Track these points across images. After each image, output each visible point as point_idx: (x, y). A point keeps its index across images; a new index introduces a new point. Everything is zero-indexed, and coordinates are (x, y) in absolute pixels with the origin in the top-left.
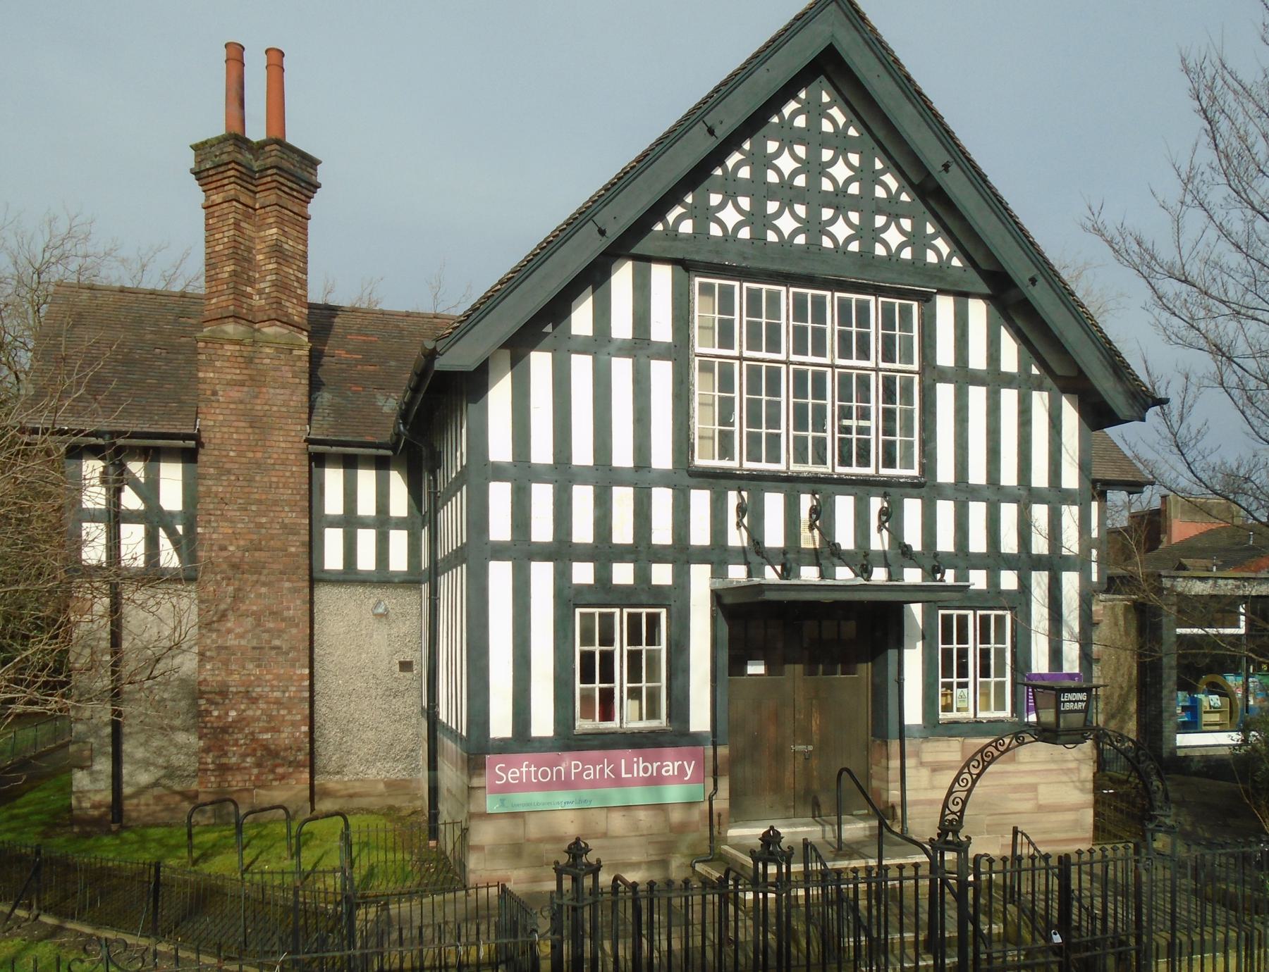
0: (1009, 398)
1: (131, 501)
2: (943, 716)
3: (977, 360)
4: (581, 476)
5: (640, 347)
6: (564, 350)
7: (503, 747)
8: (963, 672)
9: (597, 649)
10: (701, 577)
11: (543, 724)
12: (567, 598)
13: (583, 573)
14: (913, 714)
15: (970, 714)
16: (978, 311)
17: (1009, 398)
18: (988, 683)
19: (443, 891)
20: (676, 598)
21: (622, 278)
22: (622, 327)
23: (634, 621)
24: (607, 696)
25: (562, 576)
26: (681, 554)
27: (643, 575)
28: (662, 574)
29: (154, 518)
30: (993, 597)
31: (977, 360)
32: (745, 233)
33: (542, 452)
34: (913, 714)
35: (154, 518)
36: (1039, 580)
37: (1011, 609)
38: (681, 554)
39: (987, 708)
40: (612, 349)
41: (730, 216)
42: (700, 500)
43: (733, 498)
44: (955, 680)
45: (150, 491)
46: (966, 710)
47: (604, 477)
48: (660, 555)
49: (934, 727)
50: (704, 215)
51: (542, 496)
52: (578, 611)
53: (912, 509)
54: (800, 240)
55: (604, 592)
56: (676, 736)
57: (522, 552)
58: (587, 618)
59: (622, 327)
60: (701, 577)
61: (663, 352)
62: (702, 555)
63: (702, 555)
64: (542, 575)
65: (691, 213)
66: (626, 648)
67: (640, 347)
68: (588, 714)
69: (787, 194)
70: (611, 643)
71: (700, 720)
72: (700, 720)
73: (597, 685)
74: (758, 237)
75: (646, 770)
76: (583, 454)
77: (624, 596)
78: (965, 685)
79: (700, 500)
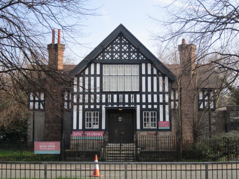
0: (155, 78)
1: (37, 99)
2: (144, 128)
3: (149, 72)
4: (149, 93)
5: (95, 75)
6: (84, 76)
7: (75, 130)
8: (148, 121)
9: (89, 117)
10: (104, 106)
11: (80, 127)
12: (84, 110)
13: (86, 107)
14: (138, 127)
15: (149, 128)
16: (149, 65)
17: (155, 78)
18: (153, 123)
19: (164, 152)
20: (101, 109)
21: (92, 66)
22: (92, 72)
23: (94, 113)
24: (90, 124)
25: (141, 107)
26: (101, 103)
27: (95, 107)
28: (155, 106)
29: (40, 101)
30: (153, 109)
31: (149, 72)
32: (136, 58)
33: (149, 90)
34: (138, 127)
35: (40, 101)
36: (161, 107)
37: (156, 111)
38: (101, 103)
39: (152, 127)
40: (91, 76)
41: (108, 56)
42: (104, 96)
43: (132, 95)
44: (146, 122)
45: (39, 97)
46: (149, 127)
47: (158, 93)
48: (98, 104)
49: (142, 129)
50: (104, 56)
51: (150, 96)
52: (86, 112)
53: (138, 96)
54: (119, 58)
55: (89, 109)
56: (100, 129)
57: (78, 104)
58: (87, 113)
59: (92, 72)
60: (104, 106)
61: (143, 75)
62: (104, 104)
63: (104, 104)
64: (81, 107)
65: (102, 56)
66: (151, 117)
67: (95, 75)
68: (87, 127)
69: (116, 52)
70: (91, 116)
71: (104, 127)
72: (104, 127)
73: (89, 122)
74: (112, 58)
75: (95, 134)
76: (155, 90)
77: (150, 110)
78: (148, 123)
79: (104, 96)
